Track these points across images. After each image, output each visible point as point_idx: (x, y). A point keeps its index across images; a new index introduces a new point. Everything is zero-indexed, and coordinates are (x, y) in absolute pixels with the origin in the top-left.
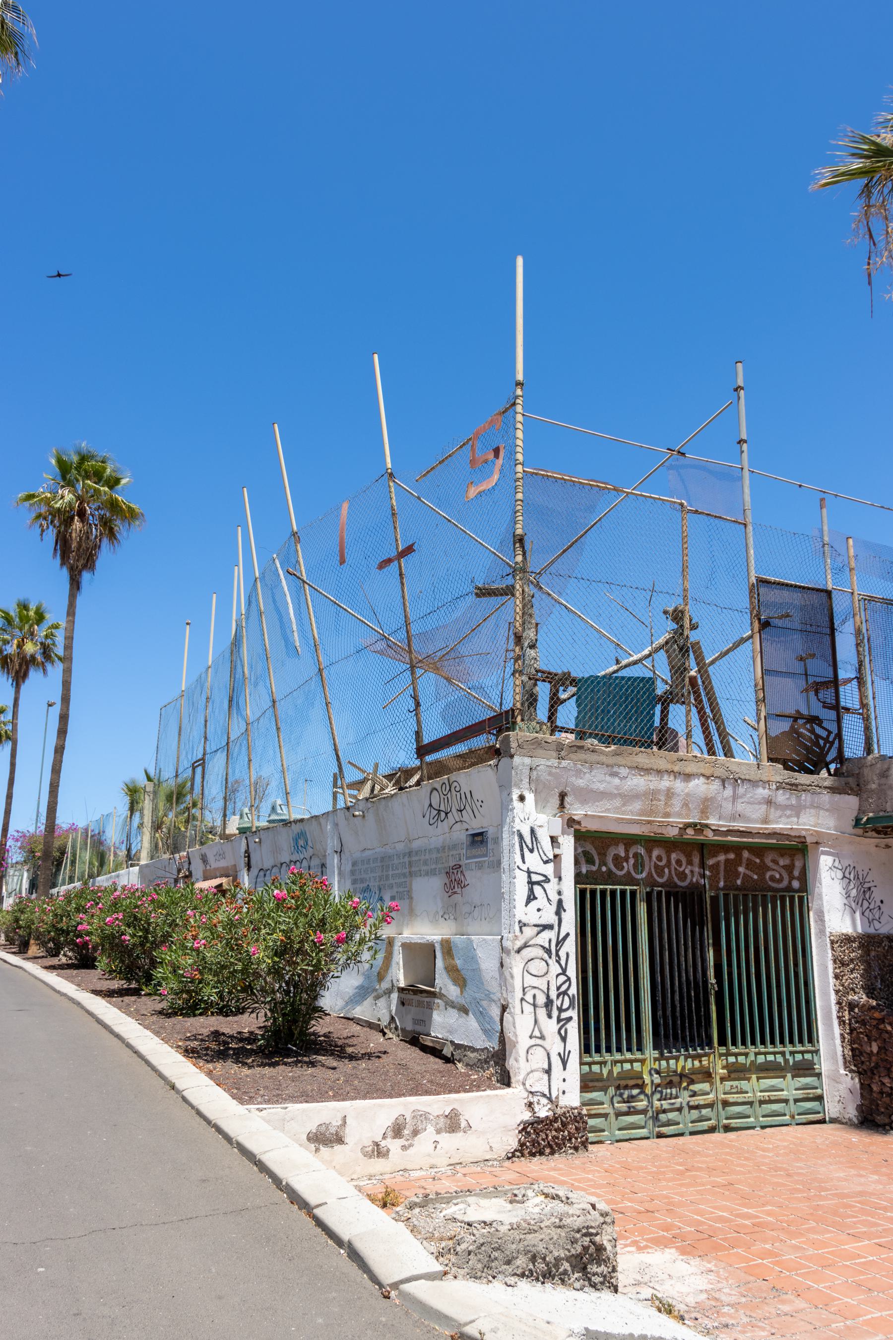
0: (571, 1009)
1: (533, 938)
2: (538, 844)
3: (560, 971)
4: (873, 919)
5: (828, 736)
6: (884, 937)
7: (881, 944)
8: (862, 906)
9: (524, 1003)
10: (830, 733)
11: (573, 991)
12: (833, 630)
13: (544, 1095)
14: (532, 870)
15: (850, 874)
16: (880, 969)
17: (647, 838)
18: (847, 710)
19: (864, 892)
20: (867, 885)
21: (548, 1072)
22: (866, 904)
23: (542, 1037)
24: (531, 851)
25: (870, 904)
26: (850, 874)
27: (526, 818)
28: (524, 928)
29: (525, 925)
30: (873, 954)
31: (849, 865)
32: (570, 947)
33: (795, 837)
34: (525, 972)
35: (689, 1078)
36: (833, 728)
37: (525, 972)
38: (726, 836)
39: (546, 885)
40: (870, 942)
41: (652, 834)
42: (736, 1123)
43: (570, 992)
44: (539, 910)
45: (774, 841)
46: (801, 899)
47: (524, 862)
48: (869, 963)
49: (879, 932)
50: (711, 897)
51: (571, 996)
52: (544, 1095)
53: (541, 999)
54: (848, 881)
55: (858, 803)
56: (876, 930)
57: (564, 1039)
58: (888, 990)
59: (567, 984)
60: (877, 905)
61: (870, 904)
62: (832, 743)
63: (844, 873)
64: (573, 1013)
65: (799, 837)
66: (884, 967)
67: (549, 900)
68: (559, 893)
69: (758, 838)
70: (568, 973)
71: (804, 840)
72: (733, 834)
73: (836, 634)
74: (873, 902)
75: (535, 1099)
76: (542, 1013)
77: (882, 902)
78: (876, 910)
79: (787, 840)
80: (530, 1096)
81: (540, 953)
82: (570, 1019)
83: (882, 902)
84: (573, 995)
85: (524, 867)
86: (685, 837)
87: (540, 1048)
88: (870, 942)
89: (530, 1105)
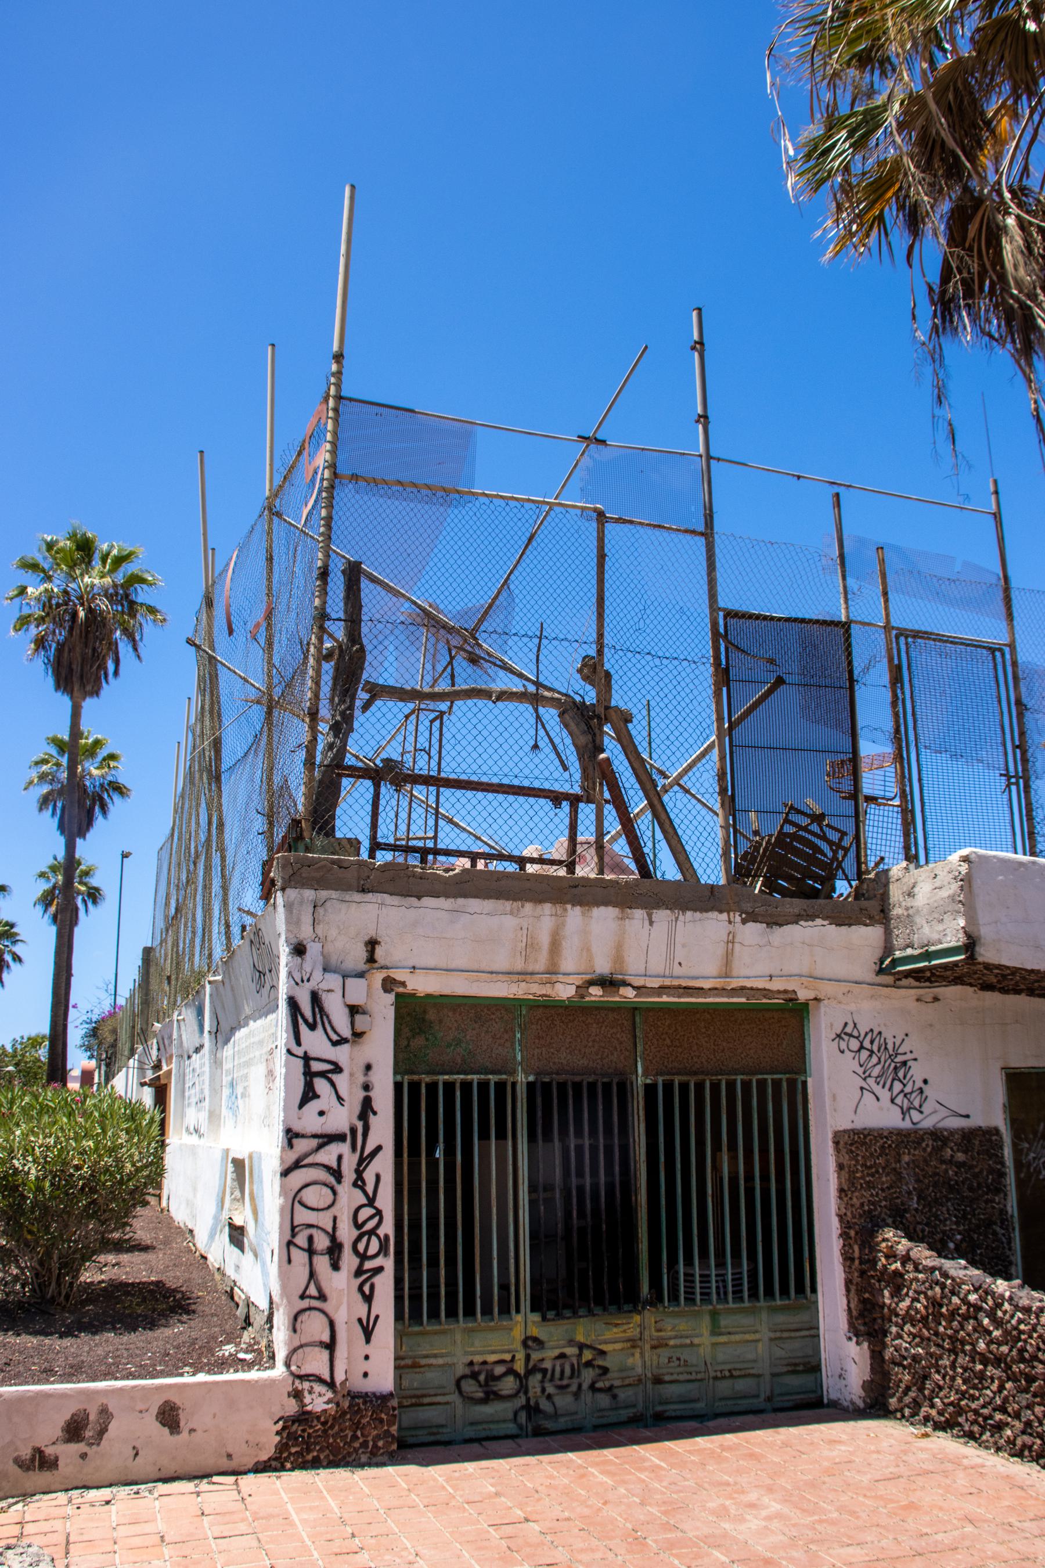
0: (382, 1255)
1: (310, 1154)
2: (325, 1018)
3: (365, 1201)
4: (909, 1109)
5: (841, 839)
6: (925, 1133)
7: (919, 1144)
8: (891, 1089)
9: (293, 1249)
10: (844, 834)
11: (388, 1228)
12: (852, 680)
13: (320, 1380)
14: (312, 1054)
15: (872, 1042)
16: (918, 1181)
17: (532, 1003)
18: (871, 799)
19: (896, 1068)
20: (900, 1059)
21: (330, 1346)
22: (897, 1086)
23: (322, 1297)
24: (312, 1027)
25: (905, 1085)
26: (872, 1042)
27: (305, 979)
28: (295, 1141)
29: (297, 1135)
30: (906, 1158)
31: (872, 1030)
32: (384, 1165)
33: (779, 992)
34: (297, 1204)
35: (595, 1349)
36: (849, 826)
37: (297, 1204)
38: (660, 995)
39: (334, 1077)
40: (903, 1142)
41: (531, 997)
42: (675, 1410)
43: (381, 1232)
44: (321, 1113)
45: (743, 1000)
46: (792, 1083)
47: (299, 1043)
48: (900, 1173)
49: (919, 1126)
50: (646, 1086)
51: (382, 1236)
52: (320, 1380)
53: (322, 1242)
54: (868, 1053)
55: (883, 938)
56: (913, 1123)
57: (368, 1299)
58: (930, 1211)
59: (376, 1219)
60: (917, 1087)
61: (905, 1085)
62: (846, 850)
63: (861, 1043)
64: (388, 1263)
65: (786, 992)
66: (924, 1177)
67: (339, 1098)
68: (367, 1087)
69: (717, 996)
70: (378, 1204)
71: (793, 996)
72: (672, 992)
73: (856, 687)
74: (911, 1083)
75: (306, 1385)
76: (322, 1263)
77: (925, 1082)
78: (914, 1095)
79: (765, 997)
80: (297, 1382)
81: (322, 1175)
82: (380, 1270)
83: (925, 1082)
84: (387, 1237)
85: (299, 1051)
86: (587, 999)
87: (317, 1313)
88: (903, 1142)
89: (297, 1395)
